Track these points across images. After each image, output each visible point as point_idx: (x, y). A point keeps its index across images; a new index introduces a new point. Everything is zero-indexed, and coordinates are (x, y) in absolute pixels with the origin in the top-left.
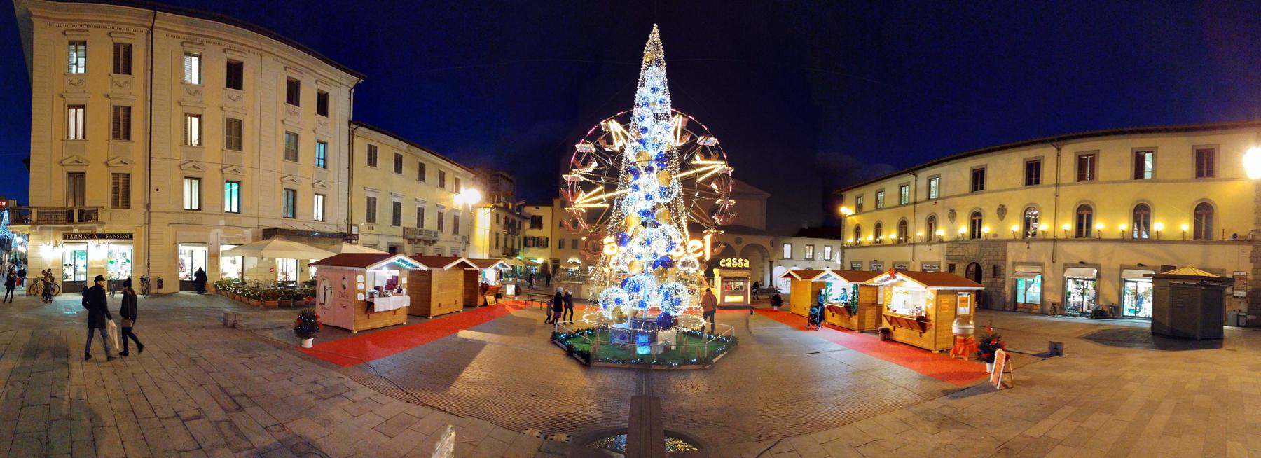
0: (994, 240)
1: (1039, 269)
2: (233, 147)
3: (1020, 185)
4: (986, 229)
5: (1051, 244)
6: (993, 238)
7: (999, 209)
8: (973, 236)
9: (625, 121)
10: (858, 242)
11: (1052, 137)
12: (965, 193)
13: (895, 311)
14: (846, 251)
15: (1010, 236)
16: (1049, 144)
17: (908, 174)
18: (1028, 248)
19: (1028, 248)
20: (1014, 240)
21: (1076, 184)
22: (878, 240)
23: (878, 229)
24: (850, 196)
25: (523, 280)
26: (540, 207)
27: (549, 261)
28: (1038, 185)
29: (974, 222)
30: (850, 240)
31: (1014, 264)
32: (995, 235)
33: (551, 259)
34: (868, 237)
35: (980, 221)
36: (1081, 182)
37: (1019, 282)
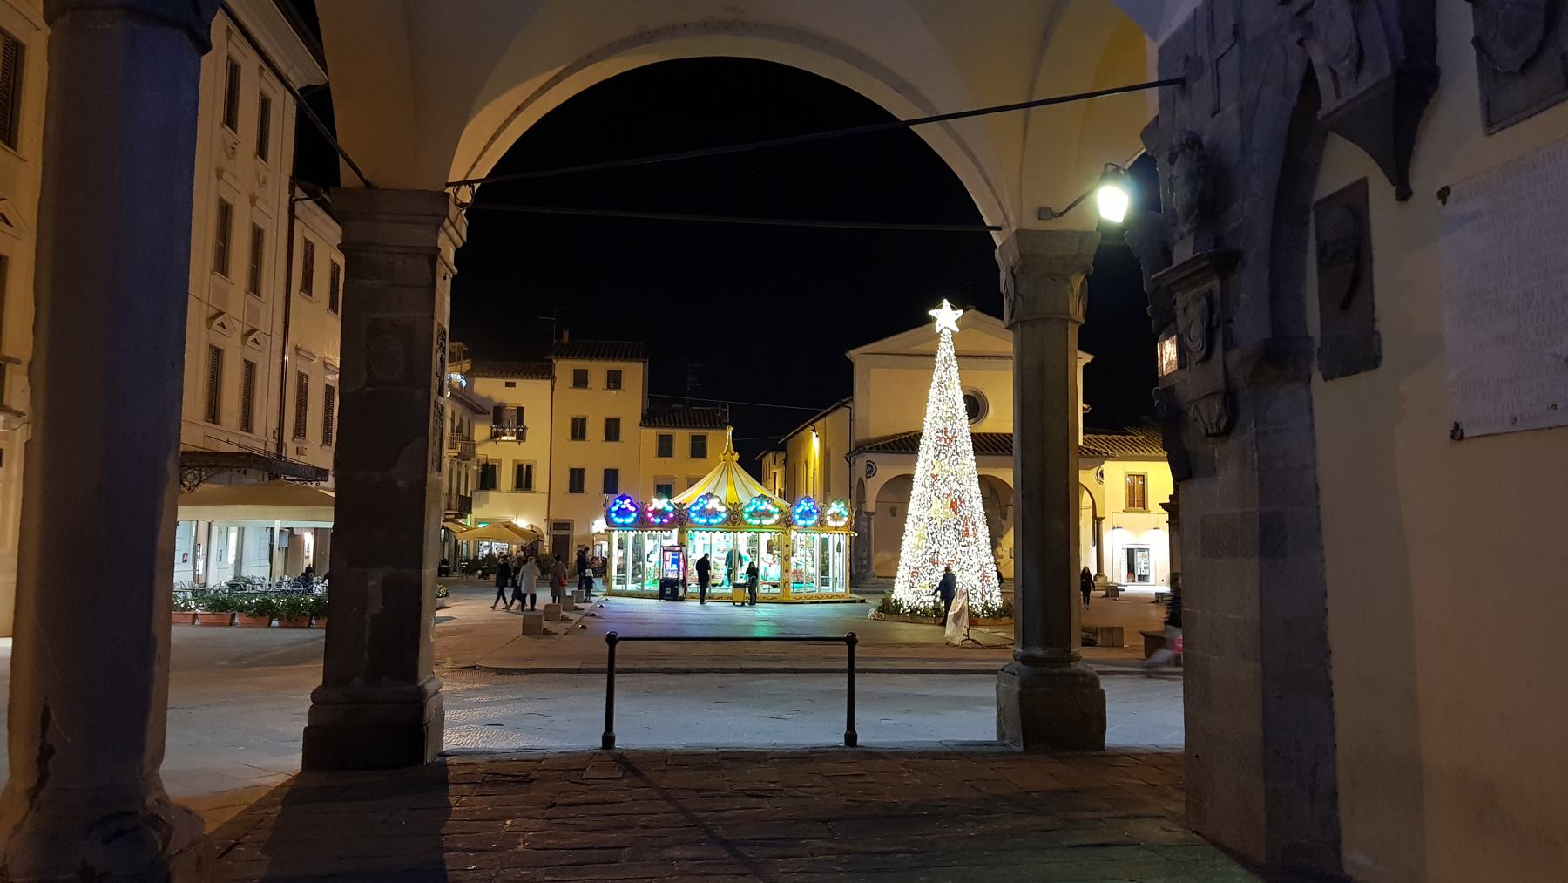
2: (556, 532)
9: (953, 332)
13: (508, 385)
25: (1180, 834)
26: (519, 382)
27: (543, 527)
33: (548, 520)
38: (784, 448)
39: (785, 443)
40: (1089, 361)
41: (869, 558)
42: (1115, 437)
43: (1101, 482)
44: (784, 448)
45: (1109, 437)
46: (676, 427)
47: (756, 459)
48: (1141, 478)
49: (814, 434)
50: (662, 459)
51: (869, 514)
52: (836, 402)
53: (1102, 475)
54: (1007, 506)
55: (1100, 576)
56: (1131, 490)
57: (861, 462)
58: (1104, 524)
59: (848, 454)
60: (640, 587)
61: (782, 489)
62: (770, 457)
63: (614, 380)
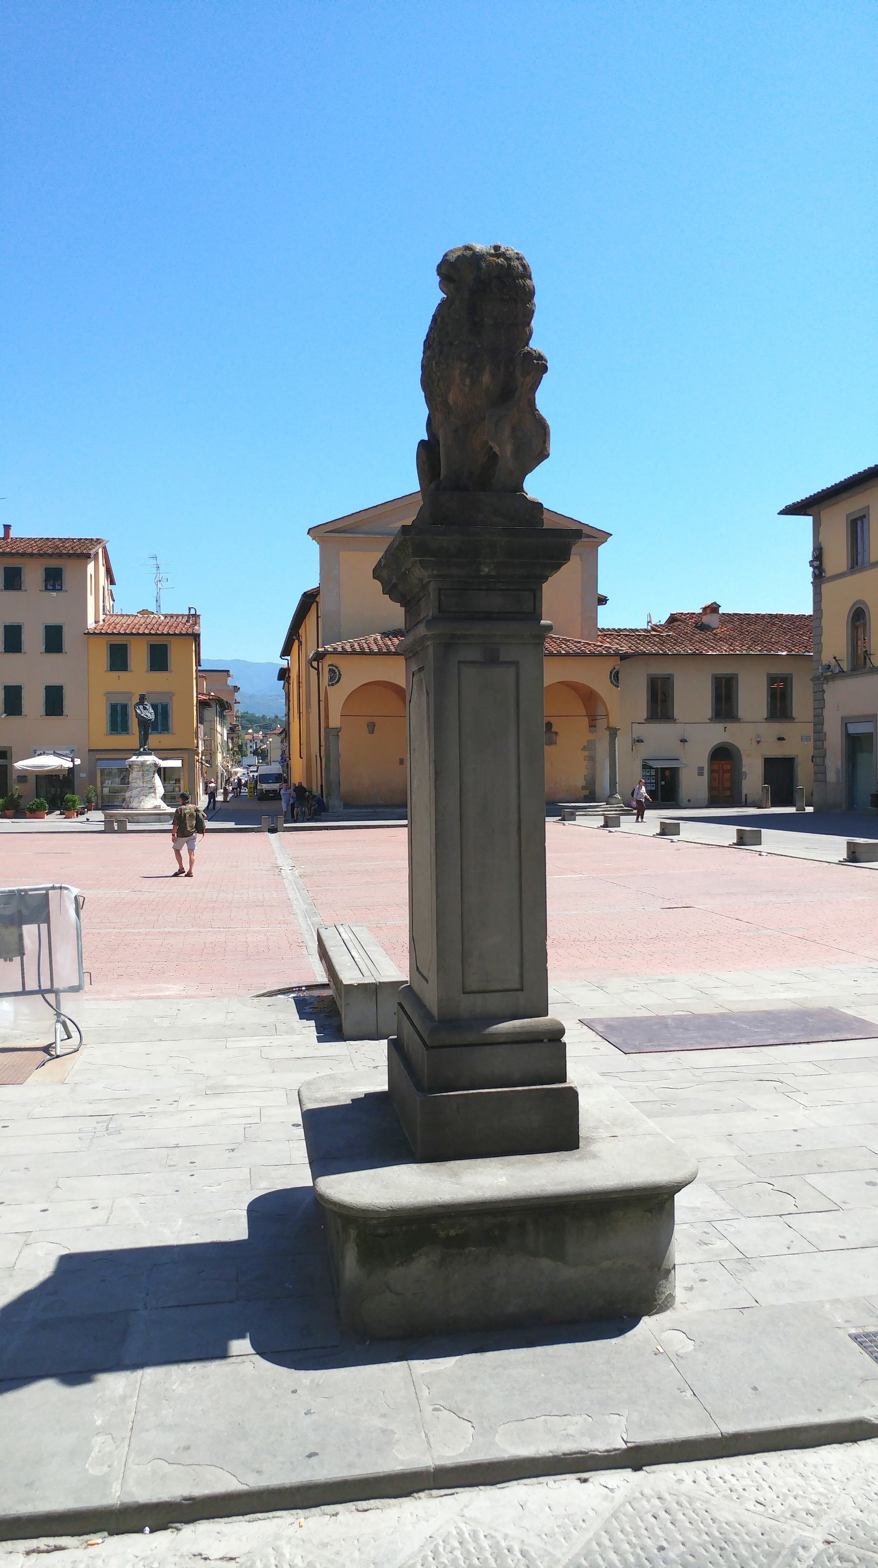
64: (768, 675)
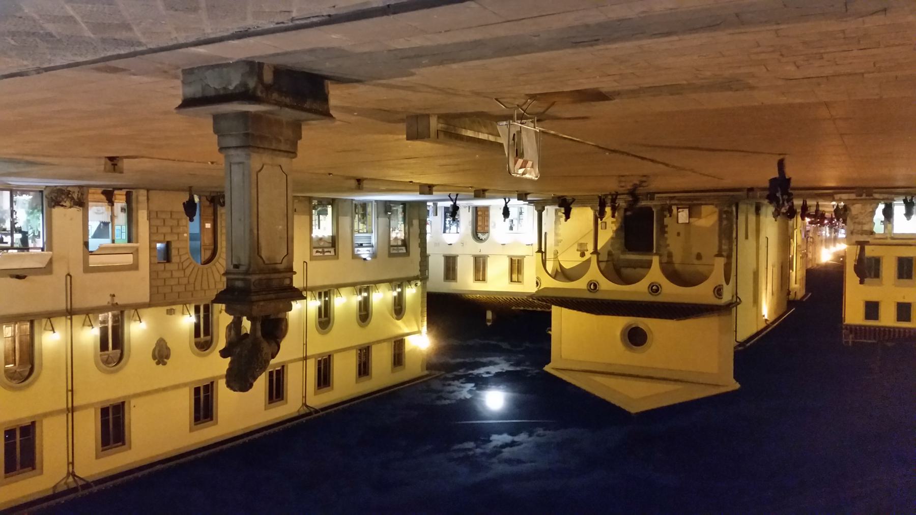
0: (174, 303)
1: (94, 261)
3: (133, 402)
4: (187, 321)
5: (77, 305)
6: (174, 307)
7: (168, 357)
8: (207, 308)
10: (399, 290)
11: (86, 492)
12: (339, 354)
14: (417, 272)
15: (146, 313)
16: (90, 480)
17: (317, 408)
18: (114, 296)
19: (114, 296)
20: (137, 307)
21: (38, 416)
22: (365, 294)
23: (364, 313)
24: (413, 369)
28: (9, 427)
29: (207, 332)
30: (411, 293)
31: (134, 267)
32: (170, 312)
34: (381, 297)
35: (197, 333)
36: (27, 422)
37: (125, 236)
38: (791, 303)
39: (789, 309)
40: (546, 366)
41: (720, 219)
42: (531, 309)
43: (538, 278)
44: (791, 303)
45: (535, 309)
46: (894, 328)
47: (810, 294)
48: (513, 280)
49: (766, 317)
50: (906, 301)
51: (719, 255)
52: (749, 347)
53: (537, 283)
54: (607, 261)
55: (539, 210)
56: (519, 271)
57: (727, 297)
58: (536, 248)
59: (739, 304)
60: (27, 198)
61: (791, 271)
62: (799, 296)
63: (872, 309)
64: (457, 282)
